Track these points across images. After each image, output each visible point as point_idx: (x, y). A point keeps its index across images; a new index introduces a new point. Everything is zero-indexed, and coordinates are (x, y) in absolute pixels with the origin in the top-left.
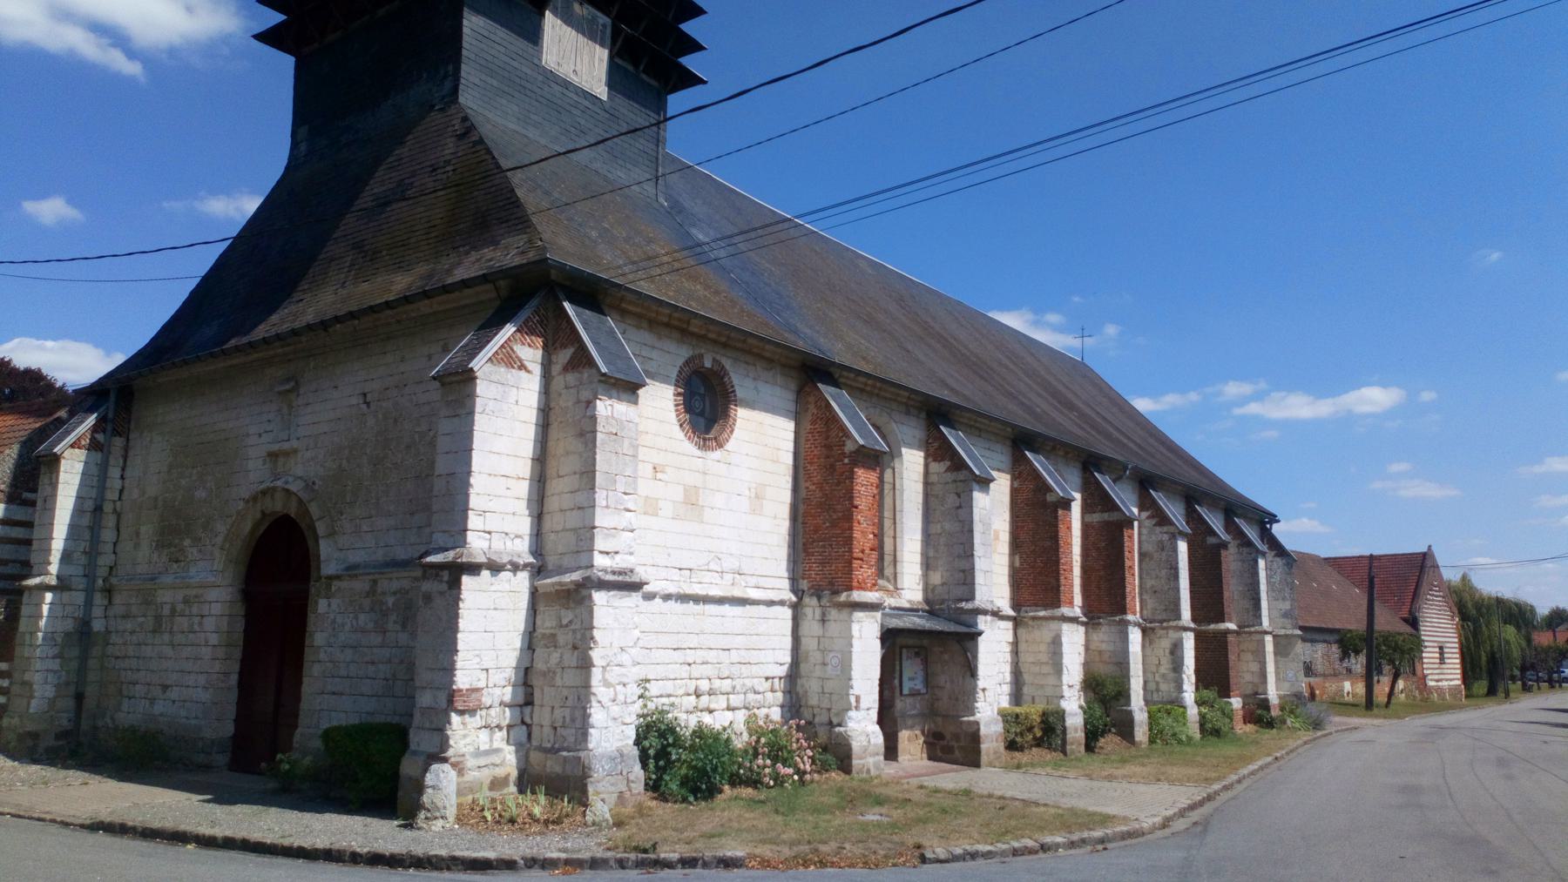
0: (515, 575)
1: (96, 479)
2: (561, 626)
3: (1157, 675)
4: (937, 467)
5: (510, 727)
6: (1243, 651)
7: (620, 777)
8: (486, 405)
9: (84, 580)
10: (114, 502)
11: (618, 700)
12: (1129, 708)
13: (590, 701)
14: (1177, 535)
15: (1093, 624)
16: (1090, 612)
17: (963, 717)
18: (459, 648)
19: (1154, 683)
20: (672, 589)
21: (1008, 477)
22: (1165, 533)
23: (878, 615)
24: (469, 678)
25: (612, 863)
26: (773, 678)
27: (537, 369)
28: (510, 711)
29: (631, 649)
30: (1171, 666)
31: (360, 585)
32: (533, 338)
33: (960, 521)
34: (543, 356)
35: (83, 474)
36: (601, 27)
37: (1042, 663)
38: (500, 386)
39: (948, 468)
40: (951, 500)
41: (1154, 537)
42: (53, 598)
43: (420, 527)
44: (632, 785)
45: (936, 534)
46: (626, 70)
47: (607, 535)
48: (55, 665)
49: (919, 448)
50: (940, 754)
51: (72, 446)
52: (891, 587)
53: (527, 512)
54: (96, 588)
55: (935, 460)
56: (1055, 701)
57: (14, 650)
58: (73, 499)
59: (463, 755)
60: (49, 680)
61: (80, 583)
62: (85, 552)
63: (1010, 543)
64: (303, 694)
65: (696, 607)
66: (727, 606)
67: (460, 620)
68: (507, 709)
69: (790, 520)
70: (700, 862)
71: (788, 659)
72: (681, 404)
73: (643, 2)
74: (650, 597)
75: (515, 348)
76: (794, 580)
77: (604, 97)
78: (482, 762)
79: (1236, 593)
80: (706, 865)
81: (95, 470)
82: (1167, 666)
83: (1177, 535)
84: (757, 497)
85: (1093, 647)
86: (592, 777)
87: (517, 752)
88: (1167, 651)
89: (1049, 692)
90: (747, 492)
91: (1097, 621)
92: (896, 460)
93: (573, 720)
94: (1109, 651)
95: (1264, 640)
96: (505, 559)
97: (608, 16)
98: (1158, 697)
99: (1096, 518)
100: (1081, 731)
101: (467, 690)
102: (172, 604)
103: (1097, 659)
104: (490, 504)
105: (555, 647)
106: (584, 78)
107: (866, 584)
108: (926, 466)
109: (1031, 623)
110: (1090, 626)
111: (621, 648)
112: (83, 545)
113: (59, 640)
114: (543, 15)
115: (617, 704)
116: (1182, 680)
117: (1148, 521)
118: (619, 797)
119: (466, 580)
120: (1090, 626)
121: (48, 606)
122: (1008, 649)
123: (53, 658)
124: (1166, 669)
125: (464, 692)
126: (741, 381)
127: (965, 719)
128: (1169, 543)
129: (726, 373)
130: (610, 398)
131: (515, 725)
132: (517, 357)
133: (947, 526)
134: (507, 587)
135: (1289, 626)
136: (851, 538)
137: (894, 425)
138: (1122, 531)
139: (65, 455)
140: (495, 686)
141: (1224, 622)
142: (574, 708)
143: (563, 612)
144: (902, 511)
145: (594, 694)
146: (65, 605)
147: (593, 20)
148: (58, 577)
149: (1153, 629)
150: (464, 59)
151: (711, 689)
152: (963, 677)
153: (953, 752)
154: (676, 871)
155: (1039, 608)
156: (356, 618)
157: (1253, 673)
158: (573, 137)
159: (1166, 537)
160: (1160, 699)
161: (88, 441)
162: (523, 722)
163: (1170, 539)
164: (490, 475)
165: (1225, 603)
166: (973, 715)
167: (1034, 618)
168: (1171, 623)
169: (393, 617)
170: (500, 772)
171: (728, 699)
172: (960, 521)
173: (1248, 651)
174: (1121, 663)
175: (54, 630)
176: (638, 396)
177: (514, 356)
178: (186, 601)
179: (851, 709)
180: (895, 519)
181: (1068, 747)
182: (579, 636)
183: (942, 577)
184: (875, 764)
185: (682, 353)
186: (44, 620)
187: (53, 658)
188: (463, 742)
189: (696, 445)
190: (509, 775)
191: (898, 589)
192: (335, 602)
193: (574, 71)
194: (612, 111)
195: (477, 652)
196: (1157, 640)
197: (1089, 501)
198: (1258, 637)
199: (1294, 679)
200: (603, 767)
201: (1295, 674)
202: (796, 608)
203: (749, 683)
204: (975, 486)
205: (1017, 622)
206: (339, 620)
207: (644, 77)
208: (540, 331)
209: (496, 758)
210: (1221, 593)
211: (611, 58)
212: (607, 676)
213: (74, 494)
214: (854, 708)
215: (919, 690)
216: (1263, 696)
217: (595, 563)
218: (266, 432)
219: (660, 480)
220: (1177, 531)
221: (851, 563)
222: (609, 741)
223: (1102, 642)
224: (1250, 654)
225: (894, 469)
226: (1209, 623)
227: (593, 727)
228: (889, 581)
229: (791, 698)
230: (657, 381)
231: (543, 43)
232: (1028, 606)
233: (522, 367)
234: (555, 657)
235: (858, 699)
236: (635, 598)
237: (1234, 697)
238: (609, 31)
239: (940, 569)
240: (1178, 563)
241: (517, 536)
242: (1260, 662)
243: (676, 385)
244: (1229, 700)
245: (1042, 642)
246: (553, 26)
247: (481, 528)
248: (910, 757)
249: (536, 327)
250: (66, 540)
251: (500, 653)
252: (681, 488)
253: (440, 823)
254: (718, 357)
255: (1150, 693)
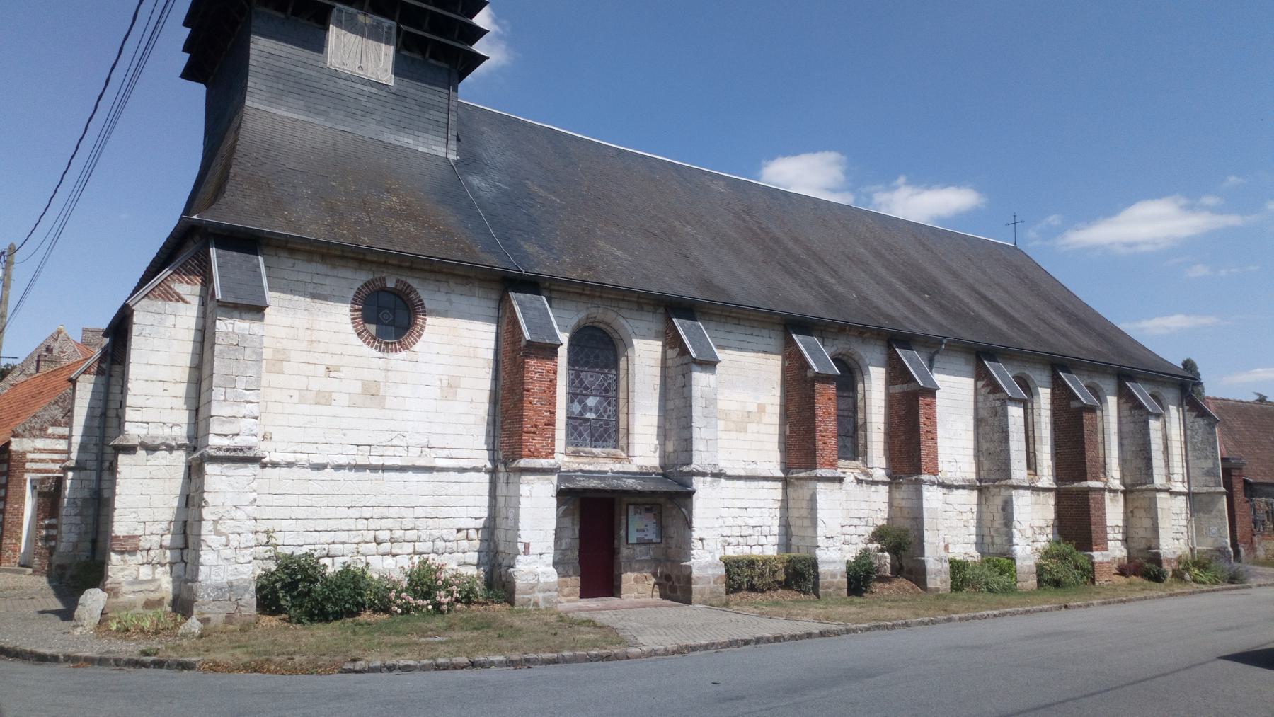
0: (171, 454)
1: (102, 395)
3: (992, 529)
4: (672, 353)
5: (172, 564)
6: (1137, 507)
7: (229, 602)
8: (143, 329)
9: (95, 463)
10: (117, 409)
11: (230, 546)
12: (923, 559)
13: (201, 546)
14: (1008, 401)
15: (896, 484)
16: (894, 473)
18: (116, 506)
19: (989, 537)
20: (343, 460)
21: (780, 357)
22: (998, 400)
23: (555, 478)
24: (127, 528)
25: (111, 661)
26: (468, 529)
27: (195, 301)
28: (171, 552)
29: (247, 507)
30: (1003, 522)
32: (191, 277)
33: (685, 398)
34: (201, 290)
35: (93, 392)
36: (385, 30)
37: (804, 517)
38: (156, 315)
39: (678, 354)
40: (680, 380)
41: (988, 404)
42: (74, 475)
44: (242, 608)
45: (671, 409)
46: (413, 60)
47: (224, 421)
48: (77, 520)
49: (656, 338)
50: (669, 593)
51: (84, 373)
52: (624, 455)
53: (185, 407)
54: (104, 468)
55: (670, 348)
56: (812, 551)
58: (87, 409)
59: (120, 583)
60: (72, 530)
61: (92, 464)
62: (96, 444)
63: (780, 414)
65: (373, 474)
66: (411, 473)
67: (117, 487)
68: (168, 552)
69: (490, 403)
70: (166, 664)
71: (486, 515)
72: (359, 318)
73: (417, 3)
74: (264, 466)
75: (172, 286)
76: (493, 451)
77: (391, 83)
78: (137, 588)
79: (1129, 453)
80: (169, 667)
81: (102, 389)
82: (999, 522)
83: (1008, 401)
84: (450, 386)
85: (896, 503)
86: (196, 601)
87: (174, 581)
88: (1000, 508)
89: (808, 542)
90: (438, 383)
91: (897, 481)
92: (629, 350)
94: (908, 508)
95: (1155, 498)
96: (158, 442)
97: (393, 20)
98: (994, 549)
99: (898, 389)
100: (842, 577)
101: (123, 537)
103: (899, 514)
104: (147, 402)
106: (370, 70)
107: (540, 453)
108: (664, 352)
109: (796, 483)
110: (894, 485)
111: (235, 506)
112: (94, 440)
113: (79, 503)
114: (327, 29)
115: (230, 548)
116: (1012, 534)
117: (983, 390)
118: (226, 617)
119: (122, 458)
120: (894, 485)
121: (70, 481)
122: (778, 505)
123: (75, 515)
124: (999, 524)
125: (121, 538)
126: (426, 293)
127: (684, 563)
128: (1001, 408)
129: (413, 290)
130: (231, 318)
131: (176, 563)
132: (175, 292)
133: (677, 402)
134: (164, 462)
135: (1212, 484)
136: (521, 416)
137: (623, 321)
138: (918, 400)
139: (80, 378)
140: (152, 534)
141: (1086, 480)
144: (634, 392)
145: (204, 541)
146: (82, 480)
147: (379, 24)
148: (77, 462)
149: (988, 488)
150: (250, 73)
151: (391, 538)
152: (684, 529)
153: (676, 592)
154: (149, 670)
155: (802, 470)
157: (1146, 528)
158: (358, 117)
159: (998, 403)
160: (995, 552)
161: (96, 369)
162: (182, 560)
163: (1001, 405)
164: (147, 381)
165: (1088, 463)
166: (690, 560)
167: (798, 479)
168: (1003, 482)
170: (156, 596)
171: (414, 545)
172: (685, 398)
173: (1141, 508)
174: (917, 518)
175: (75, 497)
176: (264, 314)
177: (171, 292)
179: (519, 554)
180: (628, 399)
181: (821, 591)
183: (674, 445)
184: (544, 599)
185: (357, 279)
186: (68, 490)
187: (75, 515)
188: (120, 574)
189: (376, 348)
190: (163, 598)
191: (628, 456)
193: (360, 67)
194: (400, 93)
195: (134, 510)
196: (991, 498)
197: (892, 374)
198: (1150, 494)
199: (1217, 535)
200: (208, 594)
201: (1219, 530)
202: (493, 472)
203: (436, 533)
204: (694, 367)
205: (786, 482)
207: (432, 61)
208: (199, 272)
209: (151, 586)
210: (1083, 454)
211: (397, 51)
212: (219, 527)
213: (87, 406)
214: (522, 554)
215: (652, 540)
216: (1155, 551)
217: (210, 443)
219: (334, 377)
220: (1007, 398)
221: (521, 436)
222: (220, 575)
223: (903, 499)
224: (1142, 510)
225: (627, 357)
226: (1073, 481)
227: (202, 565)
228: (623, 450)
229: (489, 545)
230: (331, 301)
231: (327, 50)
232: (795, 468)
233: (180, 299)
235: (527, 546)
236: (253, 469)
237: (1097, 550)
238: (394, 32)
239: (673, 439)
240: (1008, 427)
241: (174, 425)
242: (1152, 518)
243: (352, 303)
244: (1091, 553)
245: (803, 499)
246: (338, 36)
247: (140, 420)
248: (637, 595)
249: (195, 268)
250: (82, 436)
251: (155, 510)
252: (360, 383)
253: (80, 629)
254: (403, 279)
255: (987, 546)
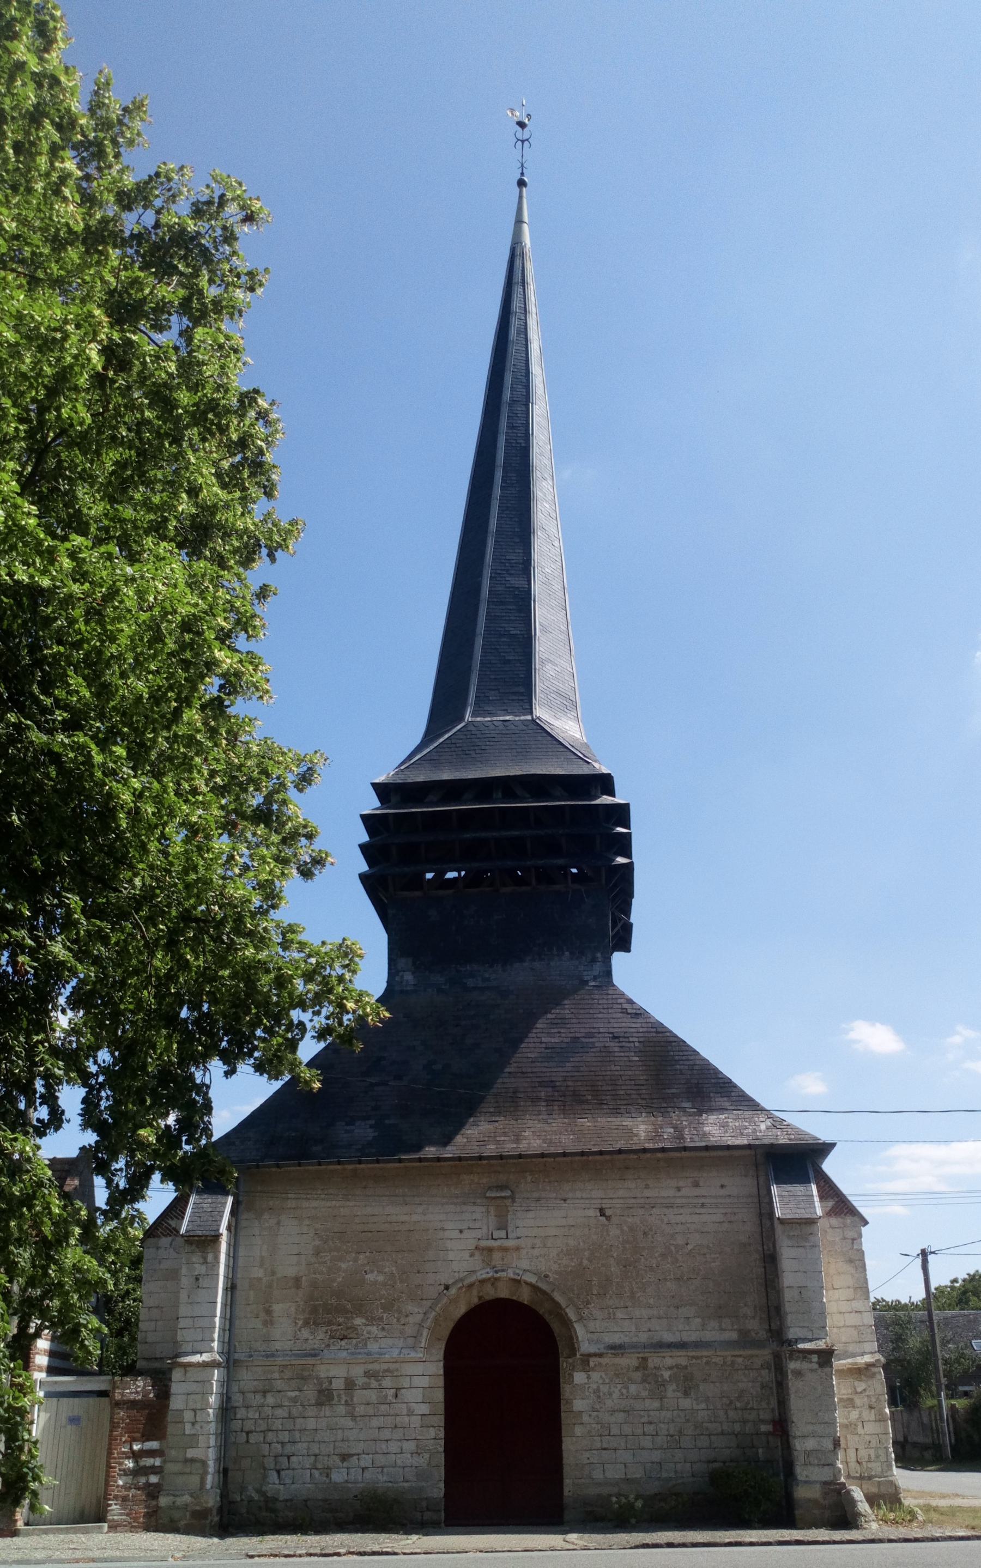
2: (857, 1393)
17: (187, 1354)
31: (629, 1361)
43: (688, 1318)
57: (166, 1427)
64: (565, 1455)
93: (877, 1457)
102: (346, 1379)
105: (854, 1407)
142: (876, 1448)
143: (856, 1383)
156: (627, 1388)
169: (671, 1388)
178: (368, 1374)
182: (874, 1400)
192: (595, 1376)
206: (604, 1389)
218: (469, 1228)
234: (854, 1415)
